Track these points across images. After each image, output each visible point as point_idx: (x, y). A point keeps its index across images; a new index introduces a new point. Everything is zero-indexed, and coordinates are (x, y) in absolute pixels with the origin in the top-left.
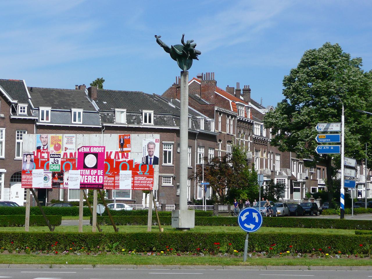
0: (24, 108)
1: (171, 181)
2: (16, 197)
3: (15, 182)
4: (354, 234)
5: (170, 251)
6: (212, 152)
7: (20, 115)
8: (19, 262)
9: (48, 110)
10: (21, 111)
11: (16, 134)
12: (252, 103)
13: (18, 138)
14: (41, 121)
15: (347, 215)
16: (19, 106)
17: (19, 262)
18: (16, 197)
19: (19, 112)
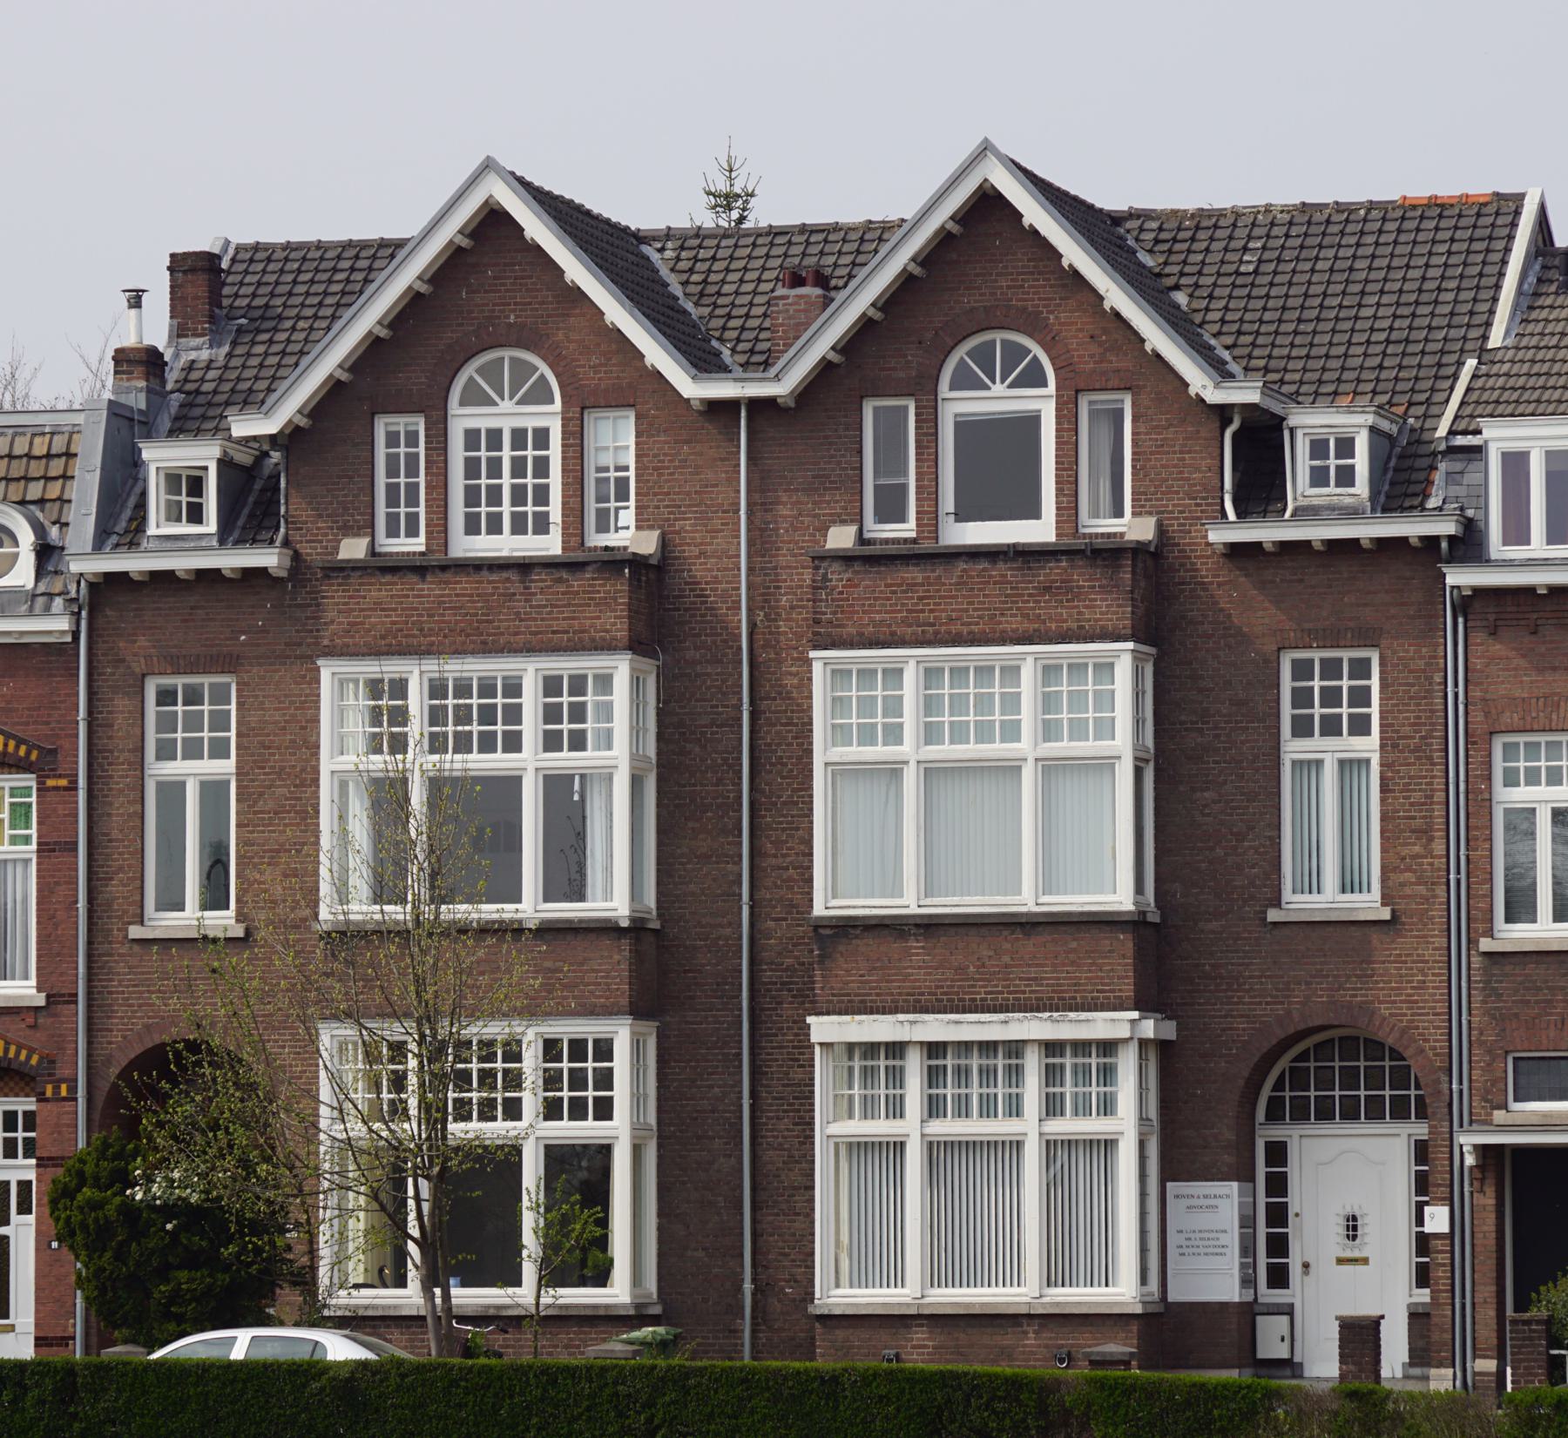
0: (1346, 447)
1: (495, 1030)
2: (1340, 1261)
3: (1326, 1128)
4: (31, 1218)
5: (396, 1238)
6: (1441, 1378)
7: (1306, 513)
8: (428, 1032)
9: (1345, 432)
10: (1319, 477)
11: (239, 735)
12: (262, 572)
13: (1302, 728)
14: (1496, 546)
15: (141, 476)
16: (1299, 434)
17: (428, 1032)
18: (1340, 1261)
19: (1299, 486)
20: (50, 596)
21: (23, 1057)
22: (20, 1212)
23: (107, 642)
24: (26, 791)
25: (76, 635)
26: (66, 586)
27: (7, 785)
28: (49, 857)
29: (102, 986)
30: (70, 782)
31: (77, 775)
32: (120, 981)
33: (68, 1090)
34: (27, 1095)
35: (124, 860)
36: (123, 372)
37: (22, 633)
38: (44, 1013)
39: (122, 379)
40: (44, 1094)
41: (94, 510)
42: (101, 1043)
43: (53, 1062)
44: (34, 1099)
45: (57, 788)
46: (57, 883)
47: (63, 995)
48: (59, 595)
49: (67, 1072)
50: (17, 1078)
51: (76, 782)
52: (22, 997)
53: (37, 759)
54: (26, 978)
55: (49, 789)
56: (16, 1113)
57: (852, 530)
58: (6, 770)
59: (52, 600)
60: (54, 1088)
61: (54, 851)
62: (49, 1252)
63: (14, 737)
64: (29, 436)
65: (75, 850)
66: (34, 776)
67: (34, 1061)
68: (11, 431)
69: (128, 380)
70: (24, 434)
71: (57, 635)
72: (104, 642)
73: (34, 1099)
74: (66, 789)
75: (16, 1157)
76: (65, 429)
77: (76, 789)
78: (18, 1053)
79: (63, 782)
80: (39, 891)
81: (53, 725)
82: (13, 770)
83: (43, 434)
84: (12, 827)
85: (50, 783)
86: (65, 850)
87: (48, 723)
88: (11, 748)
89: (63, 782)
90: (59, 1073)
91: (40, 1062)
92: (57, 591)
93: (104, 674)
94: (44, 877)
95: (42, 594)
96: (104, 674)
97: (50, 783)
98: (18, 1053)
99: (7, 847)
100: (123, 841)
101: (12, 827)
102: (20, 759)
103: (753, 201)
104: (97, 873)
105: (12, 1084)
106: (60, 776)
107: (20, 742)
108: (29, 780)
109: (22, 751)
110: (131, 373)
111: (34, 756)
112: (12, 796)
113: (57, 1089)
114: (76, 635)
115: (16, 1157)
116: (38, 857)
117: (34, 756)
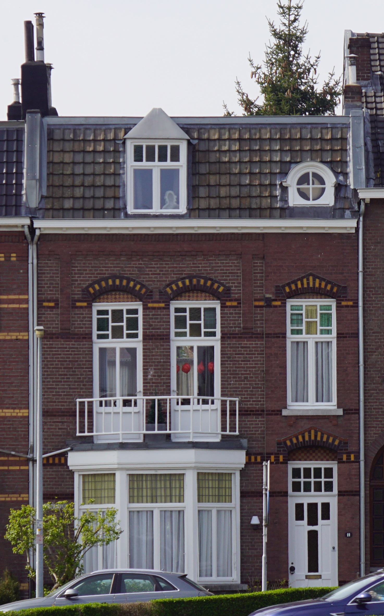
20: (343, 209)
21: (331, 440)
22: (323, 518)
23: (371, 233)
24: (329, 307)
25: (357, 229)
26: (351, 204)
27: (319, 304)
28: (343, 340)
29: (370, 406)
30: (354, 303)
31: (358, 300)
32: (380, 403)
33: (355, 457)
34: (333, 460)
35: (381, 342)
36: (349, 98)
37: (199, 228)
38: (342, 419)
39: (349, 101)
40: (342, 459)
41: (364, 167)
42: (370, 434)
43: (347, 443)
44: (336, 462)
45: (347, 306)
46: (348, 354)
47: (352, 410)
48: (348, 209)
49: (354, 449)
50: (328, 452)
51: (357, 303)
52: (330, 410)
53: (337, 291)
54: (329, 400)
55: (343, 307)
56: (310, 469)
57: (372, 180)
58: (319, 296)
59: (344, 212)
60: (347, 456)
61: (346, 337)
62: (345, 538)
63: (324, 280)
64: (320, 129)
65: (358, 337)
66: (335, 300)
67: (337, 443)
68: (309, 126)
69: (352, 101)
70: (317, 128)
71: (130, 229)
72: (370, 233)
73: (336, 462)
74: (352, 306)
75: (321, 491)
76: (338, 126)
77: (357, 307)
78: (328, 439)
79: (351, 303)
80: (338, 357)
81: (345, 274)
82: (323, 296)
83: (327, 128)
84: (321, 325)
85: (344, 303)
86: (352, 337)
87: (342, 273)
88: (323, 286)
89: (351, 303)
90: (350, 449)
91: (340, 443)
92: (347, 207)
93: (370, 249)
94: (341, 351)
95: (339, 209)
96: (370, 249)
97: (344, 303)
98: (328, 439)
99: (319, 335)
100: (381, 333)
101: (321, 325)
102: (328, 291)
103: (301, 12)
104: (367, 349)
105: (319, 454)
106: (349, 300)
107: (328, 282)
108: (332, 303)
109: (329, 287)
110: (354, 98)
111: (335, 290)
112: (321, 310)
113: (349, 458)
114: (357, 229)
115: (321, 491)
116: (337, 341)
117: (335, 290)
